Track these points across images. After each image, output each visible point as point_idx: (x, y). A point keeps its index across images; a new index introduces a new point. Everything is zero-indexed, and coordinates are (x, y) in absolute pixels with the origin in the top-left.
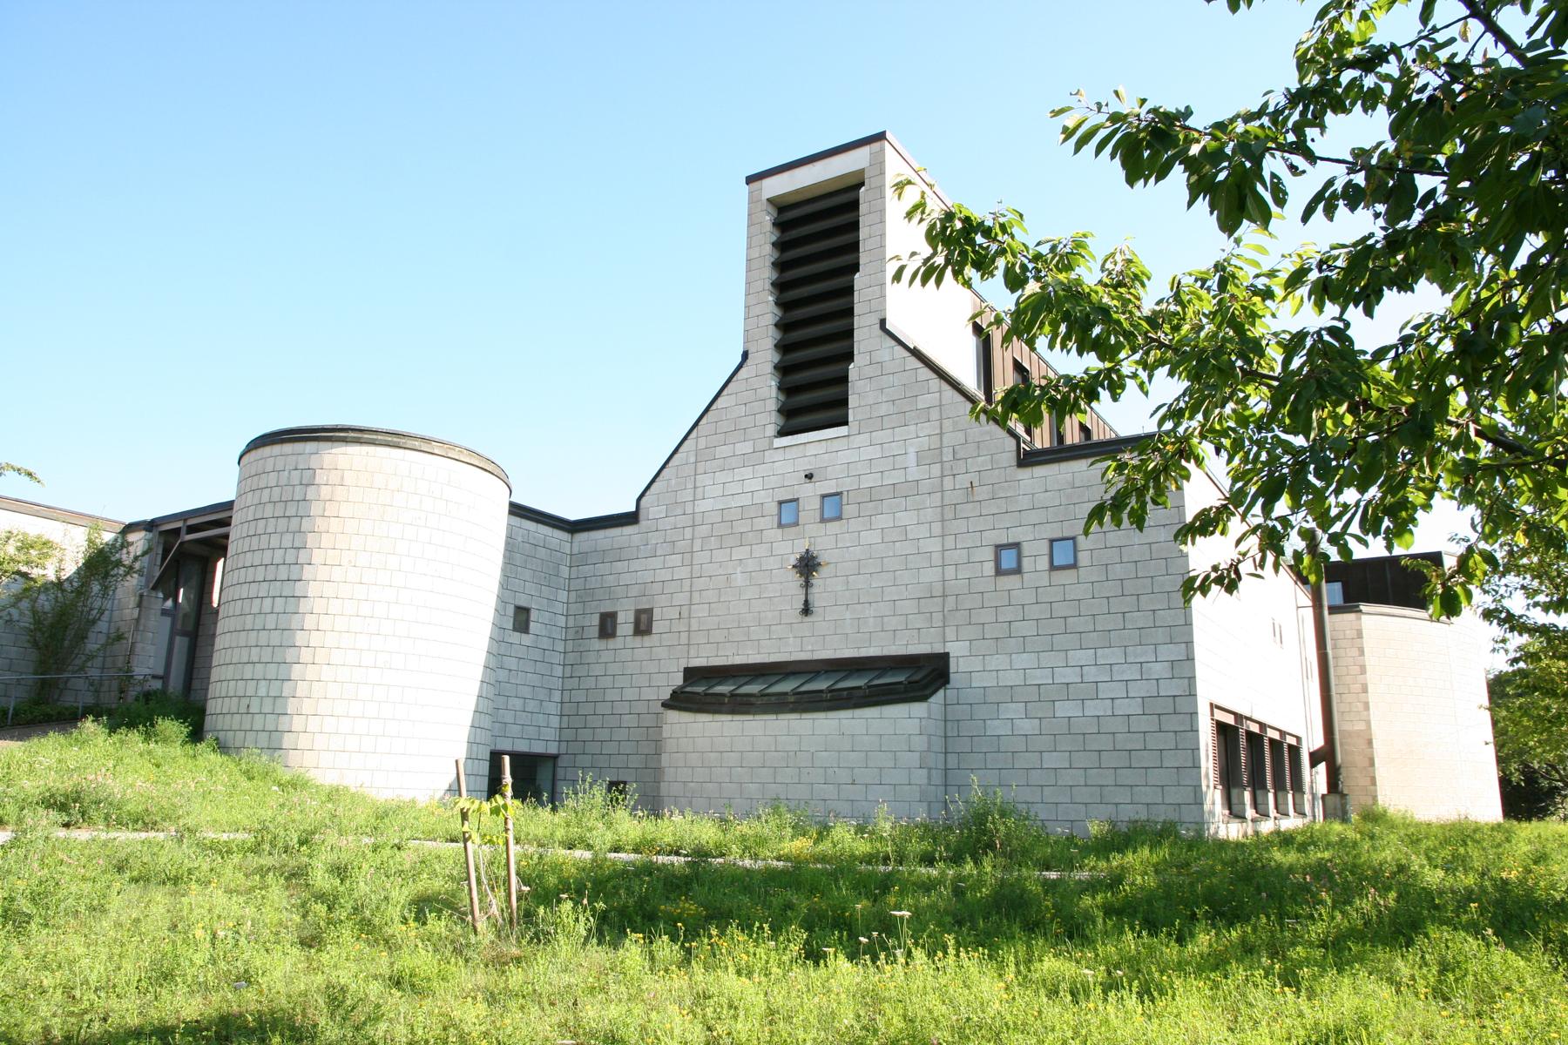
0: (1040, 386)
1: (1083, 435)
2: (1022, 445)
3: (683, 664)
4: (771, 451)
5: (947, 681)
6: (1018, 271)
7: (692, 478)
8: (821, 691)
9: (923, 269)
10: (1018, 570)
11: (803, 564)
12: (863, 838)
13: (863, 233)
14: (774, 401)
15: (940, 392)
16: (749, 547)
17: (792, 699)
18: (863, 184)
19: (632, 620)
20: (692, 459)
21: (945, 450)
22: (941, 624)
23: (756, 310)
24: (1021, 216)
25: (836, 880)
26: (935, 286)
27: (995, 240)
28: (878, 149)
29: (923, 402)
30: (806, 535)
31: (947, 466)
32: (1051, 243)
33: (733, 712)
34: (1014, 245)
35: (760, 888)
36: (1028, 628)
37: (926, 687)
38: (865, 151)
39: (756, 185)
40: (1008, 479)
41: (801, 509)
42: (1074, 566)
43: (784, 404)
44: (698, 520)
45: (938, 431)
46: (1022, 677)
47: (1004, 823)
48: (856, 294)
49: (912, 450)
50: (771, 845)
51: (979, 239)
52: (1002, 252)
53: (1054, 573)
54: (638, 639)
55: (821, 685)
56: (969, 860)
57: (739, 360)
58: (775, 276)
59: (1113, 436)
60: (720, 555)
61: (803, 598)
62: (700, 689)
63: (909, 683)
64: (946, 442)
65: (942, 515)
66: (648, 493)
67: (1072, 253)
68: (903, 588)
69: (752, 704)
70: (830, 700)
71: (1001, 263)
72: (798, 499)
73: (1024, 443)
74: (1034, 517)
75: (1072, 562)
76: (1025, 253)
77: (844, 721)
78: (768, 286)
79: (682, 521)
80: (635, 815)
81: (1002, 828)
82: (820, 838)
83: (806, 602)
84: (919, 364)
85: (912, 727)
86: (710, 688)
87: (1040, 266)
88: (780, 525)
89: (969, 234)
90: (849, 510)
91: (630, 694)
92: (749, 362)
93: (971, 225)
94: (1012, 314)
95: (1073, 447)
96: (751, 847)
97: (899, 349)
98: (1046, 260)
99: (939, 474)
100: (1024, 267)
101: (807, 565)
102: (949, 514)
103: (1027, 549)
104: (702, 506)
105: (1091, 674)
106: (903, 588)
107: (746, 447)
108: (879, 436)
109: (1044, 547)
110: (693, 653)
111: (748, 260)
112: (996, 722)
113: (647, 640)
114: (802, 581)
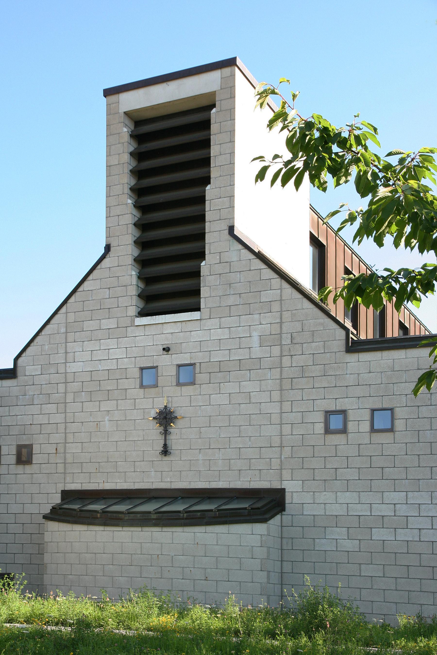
0: (382, 276)
1: (401, 332)
2: (351, 335)
3: (61, 487)
4: (132, 328)
5: (283, 509)
6: (370, 178)
7: (64, 345)
8: (179, 512)
9: (284, 171)
10: (344, 431)
11: (162, 417)
12: (217, 617)
13: (214, 150)
14: (135, 287)
15: (281, 289)
16: (115, 402)
17: (154, 516)
18: (214, 106)
19: (15, 452)
20: (63, 330)
21: (283, 336)
22: (279, 467)
23: (117, 211)
24: (375, 130)
25: (198, 645)
26: (294, 188)
27: (350, 149)
28: (229, 74)
29: (266, 296)
30: (165, 395)
31: (286, 348)
32: (400, 156)
33: (105, 524)
34: (367, 155)
35: (135, 648)
36: (352, 474)
37: (265, 513)
38: (216, 75)
39: (113, 98)
40: (338, 362)
41: (160, 374)
42: (391, 430)
43: (143, 291)
44: (70, 378)
45: (278, 321)
46: (345, 509)
47: (332, 611)
48: (207, 203)
49: (255, 334)
50: (140, 619)
51: (335, 148)
52: (356, 161)
53: (374, 435)
54: (21, 467)
55: (179, 507)
56: (304, 635)
57: (103, 251)
58: (133, 182)
59: (427, 333)
60: (89, 407)
61: (162, 442)
62: (76, 507)
63: (252, 509)
64: (284, 330)
65: (281, 386)
66: (24, 355)
67: (418, 166)
68: (248, 439)
69: (121, 519)
70: (186, 519)
71: (354, 170)
72: (157, 366)
73: (353, 333)
74: (359, 391)
75: (389, 427)
76: (376, 163)
77: (198, 535)
78: (127, 190)
79: (55, 378)
80: (25, 596)
81: (331, 614)
82: (181, 615)
83: (165, 446)
84: (263, 266)
85: (255, 541)
86: (84, 506)
87: (389, 175)
88: (142, 386)
89: (326, 143)
90: (201, 378)
91: (14, 509)
92: (111, 253)
93: (329, 135)
94: (363, 214)
95: (394, 340)
96: (125, 621)
97: (245, 252)
98: (395, 171)
99: (278, 354)
100: (375, 176)
101: (165, 418)
102: (287, 385)
103: (351, 415)
104: (73, 368)
105: (402, 510)
106: (248, 439)
107: (112, 323)
108: (227, 321)
109: (367, 415)
110: (68, 479)
111: (109, 166)
112: (324, 541)
113: (28, 469)
114: (161, 429)
